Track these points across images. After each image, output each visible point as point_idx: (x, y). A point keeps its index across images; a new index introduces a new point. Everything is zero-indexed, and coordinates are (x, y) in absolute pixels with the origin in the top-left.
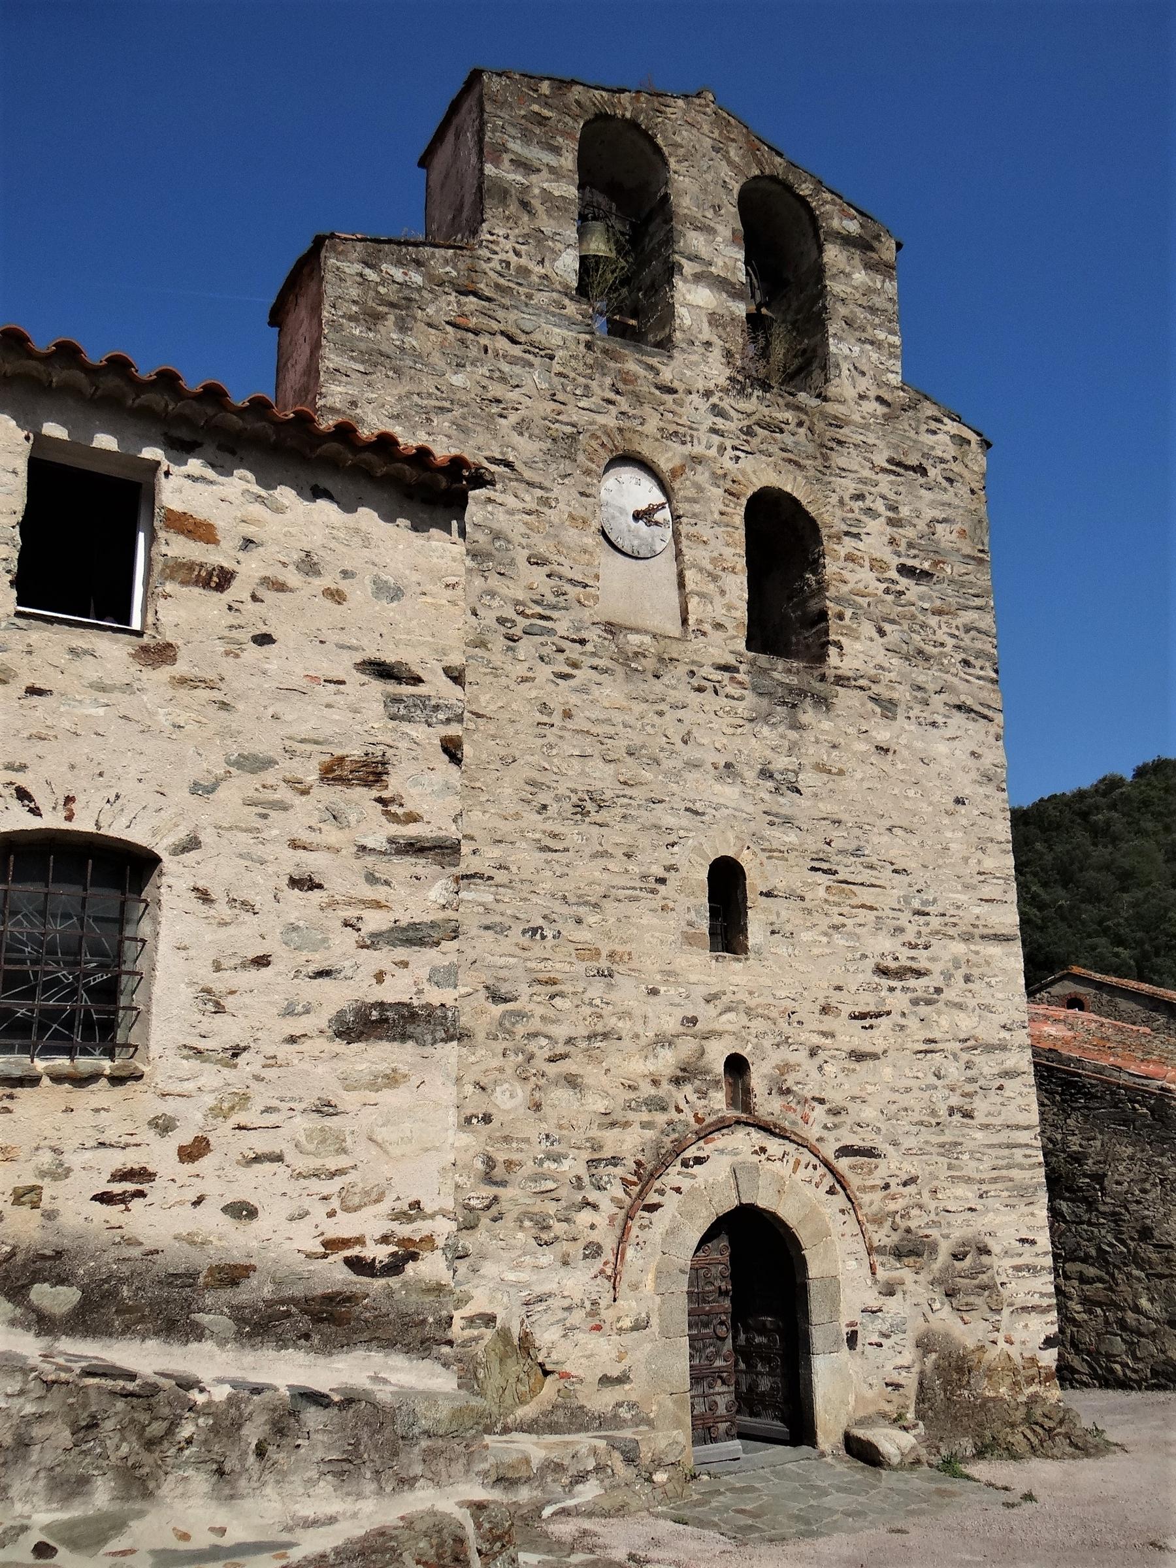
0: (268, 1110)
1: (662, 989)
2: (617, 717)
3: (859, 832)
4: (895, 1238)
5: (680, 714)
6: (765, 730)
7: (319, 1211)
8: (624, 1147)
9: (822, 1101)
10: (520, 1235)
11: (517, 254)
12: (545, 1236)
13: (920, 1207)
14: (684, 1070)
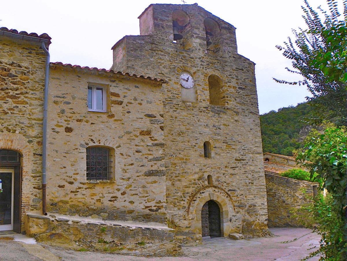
0: (135, 187)
1: (196, 165)
2: (185, 118)
3: (232, 136)
4: (239, 204)
5: (197, 116)
7: (144, 202)
9: (225, 182)
10: (171, 205)
11: (162, 36)
12: (175, 205)
13: (243, 199)
14: (200, 178)
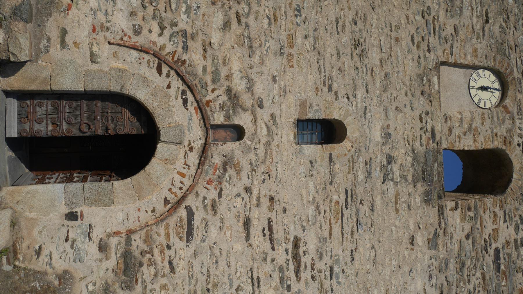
1: (276, 86)
6: (409, 159)
8: (193, 54)
9: (220, 196)
13: (156, 275)
